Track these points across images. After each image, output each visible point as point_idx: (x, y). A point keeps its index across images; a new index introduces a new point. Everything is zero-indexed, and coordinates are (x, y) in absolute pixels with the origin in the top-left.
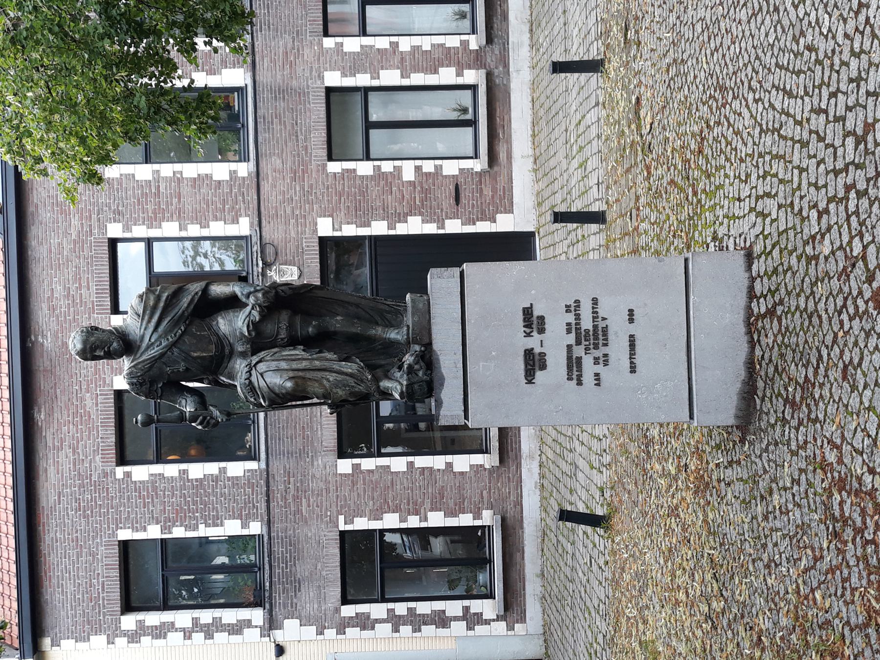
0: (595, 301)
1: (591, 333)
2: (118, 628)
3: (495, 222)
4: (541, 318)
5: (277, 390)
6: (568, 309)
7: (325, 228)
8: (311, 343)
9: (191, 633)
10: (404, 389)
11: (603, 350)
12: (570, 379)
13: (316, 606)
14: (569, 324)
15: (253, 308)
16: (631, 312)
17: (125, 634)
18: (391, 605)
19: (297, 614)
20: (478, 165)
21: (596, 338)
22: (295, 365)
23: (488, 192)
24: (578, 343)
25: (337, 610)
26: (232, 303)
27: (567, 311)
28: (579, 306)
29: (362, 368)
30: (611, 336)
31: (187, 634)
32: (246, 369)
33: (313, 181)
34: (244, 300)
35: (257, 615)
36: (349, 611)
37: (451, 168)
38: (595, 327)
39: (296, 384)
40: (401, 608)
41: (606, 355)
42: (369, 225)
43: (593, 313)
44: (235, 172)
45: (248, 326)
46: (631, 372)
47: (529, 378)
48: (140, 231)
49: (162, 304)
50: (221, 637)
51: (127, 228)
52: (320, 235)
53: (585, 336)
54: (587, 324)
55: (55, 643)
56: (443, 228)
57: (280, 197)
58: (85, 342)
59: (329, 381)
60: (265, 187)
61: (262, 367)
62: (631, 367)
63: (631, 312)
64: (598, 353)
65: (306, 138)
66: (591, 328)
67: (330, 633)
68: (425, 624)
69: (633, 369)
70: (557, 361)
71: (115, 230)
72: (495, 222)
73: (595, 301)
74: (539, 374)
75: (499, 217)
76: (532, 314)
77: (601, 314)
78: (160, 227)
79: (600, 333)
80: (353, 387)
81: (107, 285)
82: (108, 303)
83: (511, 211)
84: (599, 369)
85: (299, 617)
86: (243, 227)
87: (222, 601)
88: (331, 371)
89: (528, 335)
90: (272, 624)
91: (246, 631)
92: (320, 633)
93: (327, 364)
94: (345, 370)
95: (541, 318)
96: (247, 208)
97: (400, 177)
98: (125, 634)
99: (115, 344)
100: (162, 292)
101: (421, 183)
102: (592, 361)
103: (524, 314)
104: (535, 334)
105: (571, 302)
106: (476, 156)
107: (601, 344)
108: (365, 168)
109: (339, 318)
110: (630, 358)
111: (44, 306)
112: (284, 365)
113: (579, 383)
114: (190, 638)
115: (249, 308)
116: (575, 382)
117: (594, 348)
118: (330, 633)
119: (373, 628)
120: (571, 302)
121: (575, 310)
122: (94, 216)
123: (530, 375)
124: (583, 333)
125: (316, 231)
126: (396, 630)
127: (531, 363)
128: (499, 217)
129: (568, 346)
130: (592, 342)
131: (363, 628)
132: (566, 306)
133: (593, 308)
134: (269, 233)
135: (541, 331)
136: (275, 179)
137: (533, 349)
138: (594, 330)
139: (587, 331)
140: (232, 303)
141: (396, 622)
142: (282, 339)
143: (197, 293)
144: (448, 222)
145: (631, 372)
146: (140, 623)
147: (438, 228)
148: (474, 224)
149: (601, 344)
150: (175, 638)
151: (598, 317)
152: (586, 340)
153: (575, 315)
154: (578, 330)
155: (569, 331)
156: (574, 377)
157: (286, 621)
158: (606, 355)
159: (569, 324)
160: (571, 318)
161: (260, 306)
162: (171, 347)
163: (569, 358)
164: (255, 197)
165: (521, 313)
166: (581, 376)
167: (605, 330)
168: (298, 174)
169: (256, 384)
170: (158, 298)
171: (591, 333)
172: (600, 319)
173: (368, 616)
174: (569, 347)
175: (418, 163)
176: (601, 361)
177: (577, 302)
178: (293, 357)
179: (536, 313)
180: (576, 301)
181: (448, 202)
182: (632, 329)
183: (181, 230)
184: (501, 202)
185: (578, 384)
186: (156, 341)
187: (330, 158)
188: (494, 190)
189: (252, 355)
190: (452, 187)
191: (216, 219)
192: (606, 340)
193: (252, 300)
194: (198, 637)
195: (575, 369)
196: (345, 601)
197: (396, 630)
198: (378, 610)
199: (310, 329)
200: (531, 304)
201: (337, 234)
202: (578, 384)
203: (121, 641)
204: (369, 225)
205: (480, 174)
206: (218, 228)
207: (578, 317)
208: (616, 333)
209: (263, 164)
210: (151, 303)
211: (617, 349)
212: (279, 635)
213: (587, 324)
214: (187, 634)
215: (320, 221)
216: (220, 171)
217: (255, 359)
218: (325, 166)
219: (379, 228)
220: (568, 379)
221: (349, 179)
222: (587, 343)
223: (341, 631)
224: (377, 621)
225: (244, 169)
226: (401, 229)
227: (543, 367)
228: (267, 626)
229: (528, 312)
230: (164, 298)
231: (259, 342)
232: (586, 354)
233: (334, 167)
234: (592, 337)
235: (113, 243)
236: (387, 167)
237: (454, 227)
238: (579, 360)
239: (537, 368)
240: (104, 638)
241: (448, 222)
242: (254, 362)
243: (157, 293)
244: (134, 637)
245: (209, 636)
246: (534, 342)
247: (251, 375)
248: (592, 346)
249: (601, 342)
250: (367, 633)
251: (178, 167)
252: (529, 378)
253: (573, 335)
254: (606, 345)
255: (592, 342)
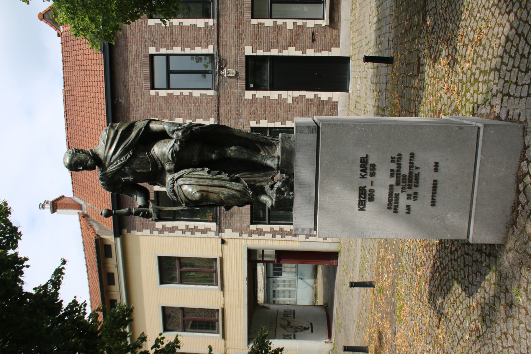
0: (412, 155)
1: (407, 177)
2: (154, 227)
3: (331, 51)
4: (373, 166)
5: (190, 198)
6: (393, 160)
7: (249, 51)
8: (213, 166)
9: (185, 232)
10: (274, 204)
11: (415, 190)
12: (389, 208)
13: (239, 225)
14: (392, 171)
15: (175, 142)
16: (437, 164)
17: (157, 230)
18: (272, 226)
19: (231, 227)
20: (324, 23)
21: (410, 181)
22: (202, 182)
23: (328, 37)
24: (398, 184)
25: (249, 227)
26: (163, 135)
27: (392, 162)
28: (400, 158)
29: (246, 187)
30: (421, 180)
31: (184, 232)
32: (171, 182)
33: (244, 29)
34: (170, 135)
35: (213, 226)
36: (254, 227)
37: (311, 24)
38: (411, 173)
39: (202, 195)
40: (277, 227)
41: (416, 193)
42: (270, 51)
43: (410, 163)
44: (207, 23)
45: (172, 154)
46: (432, 205)
47: (361, 207)
48: (163, 51)
49: (118, 137)
50: (198, 234)
51: (157, 49)
52: (246, 54)
53: (403, 179)
54: (405, 171)
55: (129, 232)
56: (305, 53)
57: (228, 36)
58: (71, 160)
59: (224, 195)
60: (222, 31)
61: (180, 182)
62: (432, 202)
63: (437, 164)
64: (410, 192)
65: (241, 8)
66: (407, 174)
67: (245, 236)
68: (287, 235)
69: (433, 204)
70: (382, 195)
71: (152, 50)
72: (331, 51)
73: (412, 155)
74: (368, 204)
75: (333, 49)
76: (367, 163)
77: (416, 164)
78: (172, 49)
79: (414, 178)
80: (240, 198)
81: (148, 76)
82: (149, 84)
83: (339, 47)
84: (411, 202)
85: (232, 228)
86: (210, 50)
87: (199, 219)
88: (225, 187)
89: (363, 177)
90: (220, 230)
91: (208, 232)
92: (241, 235)
93: (222, 183)
94: (234, 188)
95: (373, 166)
96: (212, 41)
97: (286, 28)
98: (157, 230)
99: (89, 162)
100: (119, 128)
101: (296, 31)
102: (406, 197)
103: (361, 162)
104: (368, 176)
105: (395, 155)
106: (323, 19)
107: (413, 185)
108: (269, 23)
109: (233, 148)
110: (432, 196)
111: (121, 85)
112: (193, 181)
113: (396, 211)
114: (185, 233)
115: (173, 141)
116: (392, 210)
117: (408, 188)
118: (245, 236)
119: (264, 235)
120: (395, 155)
121: (398, 161)
122: (143, 44)
123: (362, 205)
124: (402, 177)
125: (244, 53)
126: (274, 236)
127: (363, 196)
128: (333, 49)
129: (390, 186)
130: (407, 183)
131: (260, 235)
132: (392, 158)
133: (410, 160)
134: (224, 54)
135: (372, 175)
136: (226, 27)
137: (365, 187)
138: (409, 176)
139: (404, 176)
140: (163, 135)
141: (274, 233)
142: (195, 162)
143: (141, 129)
144: (308, 51)
145: (432, 205)
146: (164, 226)
147: (303, 53)
148: (321, 52)
149: (413, 185)
150: (178, 233)
151: (413, 167)
152: (403, 182)
153: (397, 164)
154: (398, 174)
155: (392, 176)
156: (393, 207)
157: (226, 230)
158: (416, 193)
159: (392, 171)
160: (394, 166)
161: (180, 140)
162: (123, 165)
163: (390, 194)
164: (216, 36)
165: (359, 161)
166: (397, 206)
167: (417, 176)
168: (237, 24)
169: (177, 192)
170: (116, 133)
171: (407, 177)
172: (414, 168)
173: (262, 230)
174: (391, 187)
175: (295, 21)
176: (412, 197)
177: (400, 155)
178: (200, 177)
179: (370, 162)
180: (398, 155)
181: (308, 41)
182: (436, 176)
183: (182, 51)
184: (334, 41)
185: (394, 212)
186: (114, 161)
187: (253, 18)
188: (331, 36)
189: (175, 173)
190: (311, 34)
191: (198, 46)
192: (417, 182)
193: (175, 136)
194: (188, 234)
195: (394, 202)
196: (252, 223)
197: (274, 236)
198: (266, 228)
199: (214, 156)
200: (367, 155)
201: (254, 54)
202: (394, 212)
203: (156, 233)
204: (270, 51)
205: (325, 27)
206: (198, 50)
207: (399, 166)
208: (425, 178)
209: (221, 19)
210: (112, 136)
211: (424, 189)
212: (224, 235)
213: (405, 171)
214: (184, 232)
215: (246, 48)
216: (200, 23)
217: (176, 175)
218: (250, 21)
219: (274, 52)
220: (388, 208)
221: (261, 28)
222: (404, 184)
223: (250, 235)
224: (266, 232)
225: (211, 22)
226: (285, 53)
227: (371, 199)
228: (218, 231)
229: (364, 161)
230: (120, 133)
231: (181, 161)
232: (402, 191)
233: (254, 22)
234: (408, 180)
235: (152, 56)
236: (280, 22)
237: (310, 53)
238: (397, 196)
239: (367, 200)
240: (148, 231)
241: (308, 51)
242: (176, 177)
243: (116, 129)
244: (161, 231)
245: (193, 233)
246: (366, 183)
247: (174, 186)
248: (407, 187)
249: (413, 184)
250: (261, 237)
251: (181, 20)
252: (361, 207)
253: (394, 179)
254: (416, 186)
255: (407, 183)
